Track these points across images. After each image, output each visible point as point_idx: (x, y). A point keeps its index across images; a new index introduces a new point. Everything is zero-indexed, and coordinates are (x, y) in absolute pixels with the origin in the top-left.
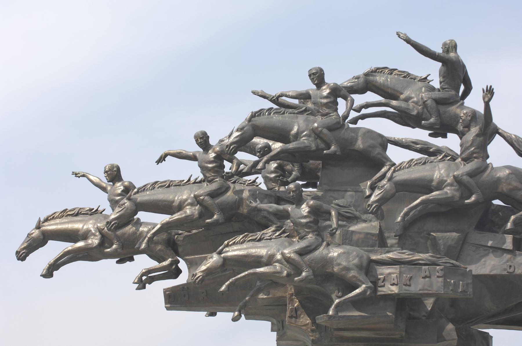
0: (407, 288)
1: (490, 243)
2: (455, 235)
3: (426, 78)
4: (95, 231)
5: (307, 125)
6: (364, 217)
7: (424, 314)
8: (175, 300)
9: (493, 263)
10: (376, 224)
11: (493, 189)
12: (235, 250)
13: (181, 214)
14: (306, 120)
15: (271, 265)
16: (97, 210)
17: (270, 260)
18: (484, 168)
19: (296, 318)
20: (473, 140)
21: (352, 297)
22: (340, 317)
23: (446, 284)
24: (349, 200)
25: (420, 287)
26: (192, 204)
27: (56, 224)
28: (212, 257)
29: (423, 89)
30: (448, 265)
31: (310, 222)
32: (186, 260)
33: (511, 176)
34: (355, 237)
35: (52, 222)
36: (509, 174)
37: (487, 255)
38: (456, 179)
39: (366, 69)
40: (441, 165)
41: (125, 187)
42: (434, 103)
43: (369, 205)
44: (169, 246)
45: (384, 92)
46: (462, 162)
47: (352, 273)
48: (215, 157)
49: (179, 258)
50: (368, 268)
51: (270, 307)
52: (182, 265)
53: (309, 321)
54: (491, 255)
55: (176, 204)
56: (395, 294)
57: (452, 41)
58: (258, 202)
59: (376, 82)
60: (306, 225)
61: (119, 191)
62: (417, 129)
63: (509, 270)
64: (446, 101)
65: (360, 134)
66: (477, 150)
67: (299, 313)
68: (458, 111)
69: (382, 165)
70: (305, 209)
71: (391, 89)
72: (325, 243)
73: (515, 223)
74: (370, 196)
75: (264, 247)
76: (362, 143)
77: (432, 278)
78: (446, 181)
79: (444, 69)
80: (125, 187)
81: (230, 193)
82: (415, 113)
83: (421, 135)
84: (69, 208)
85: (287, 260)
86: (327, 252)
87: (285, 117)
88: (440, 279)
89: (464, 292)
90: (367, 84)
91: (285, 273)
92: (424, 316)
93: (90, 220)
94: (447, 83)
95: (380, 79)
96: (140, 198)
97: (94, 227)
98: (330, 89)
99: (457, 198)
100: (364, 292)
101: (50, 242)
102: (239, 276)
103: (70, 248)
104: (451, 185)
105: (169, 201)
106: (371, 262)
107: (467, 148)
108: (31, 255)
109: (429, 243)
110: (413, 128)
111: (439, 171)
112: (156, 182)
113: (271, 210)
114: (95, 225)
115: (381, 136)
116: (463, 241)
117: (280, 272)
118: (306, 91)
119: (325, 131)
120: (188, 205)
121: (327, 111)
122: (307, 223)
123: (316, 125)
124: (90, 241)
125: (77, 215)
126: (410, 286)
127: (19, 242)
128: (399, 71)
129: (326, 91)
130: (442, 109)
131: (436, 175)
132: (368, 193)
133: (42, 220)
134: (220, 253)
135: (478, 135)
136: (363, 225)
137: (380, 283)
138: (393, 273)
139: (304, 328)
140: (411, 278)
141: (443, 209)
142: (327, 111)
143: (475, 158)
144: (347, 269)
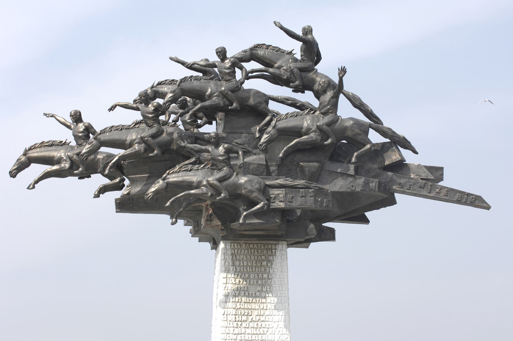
0: (290, 204)
1: (339, 170)
2: (315, 164)
3: (291, 52)
4: (66, 158)
5: (217, 88)
6: (255, 151)
7: (295, 218)
8: (124, 205)
9: (341, 183)
10: (262, 156)
11: (342, 133)
12: (173, 178)
13: (132, 150)
14: (216, 85)
15: (199, 188)
16: (65, 142)
17: (198, 185)
18: (337, 119)
19: (211, 221)
20: (329, 101)
21: (255, 210)
22: (248, 224)
23: (316, 201)
24: (244, 140)
25: (299, 203)
26: (139, 143)
27: (37, 152)
28: (159, 182)
29: (290, 60)
30: (317, 188)
31: (225, 159)
32: (129, 179)
33: (354, 126)
34: (251, 167)
35: (34, 151)
36: (353, 124)
37: (337, 178)
38: (318, 127)
39: (251, 45)
40: (308, 117)
41: (85, 126)
42: (298, 71)
43: (260, 145)
44: (119, 169)
45: (266, 62)
46: (321, 115)
47: (255, 194)
48: (153, 110)
49: (125, 177)
50: (265, 190)
51: (189, 212)
52: (127, 182)
53: (219, 223)
54: (340, 178)
55: (128, 142)
56: (282, 208)
57: (309, 26)
58: (186, 143)
59: (258, 54)
60: (223, 161)
61: (81, 130)
62: (284, 87)
63: (352, 189)
64: (302, 68)
65: (251, 94)
66: (332, 108)
67: (212, 217)
68: (314, 76)
69: (266, 115)
70: (221, 149)
71: (268, 60)
72: (235, 173)
73: (357, 157)
74: (260, 138)
75: (195, 175)
76: (253, 100)
77: (307, 197)
78: (312, 129)
79: (304, 47)
80: (85, 126)
81: (164, 135)
82: (285, 77)
83: (286, 92)
84: (46, 141)
85: (210, 185)
86: (237, 180)
87: (202, 83)
88: (312, 198)
89: (327, 206)
90: (251, 55)
91: (209, 194)
92: (295, 219)
93: (61, 149)
94: (306, 57)
95: (260, 52)
96: (102, 137)
97: (65, 155)
98: (231, 62)
99: (319, 141)
100: (263, 207)
101: (33, 165)
102: (179, 196)
103: (49, 170)
104: (315, 131)
105: (123, 141)
106: (267, 186)
107: (325, 106)
108: (19, 174)
109: (298, 169)
110: (282, 86)
111: (307, 122)
112: (113, 127)
113: (196, 149)
114: (65, 153)
115: (265, 95)
116: (321, 169)
117: (206, 194)
118: (213, 62)
119: (230, 93)
120: (136, 143)
121: (229, 78)
122: (224, 160)
123: (223, 88)
124: (63, 165)
125: (51, 145)
126: (292, 202)
127: (11, 165)
128: (273, 47)
129: (228, 63)
130: (304, 74)
131: (305, 125)
132: (257, 135)
133: (27, 149)
134: (164, 179)
135: (332, 98)
136: (254, 157)
137: (272, 200)
138: (281, 194)
139: (216, 228)
140: (292, 197)
141: (308, 147)
142: (229, 78)
143: (330, 113)
144: (251, 191)
